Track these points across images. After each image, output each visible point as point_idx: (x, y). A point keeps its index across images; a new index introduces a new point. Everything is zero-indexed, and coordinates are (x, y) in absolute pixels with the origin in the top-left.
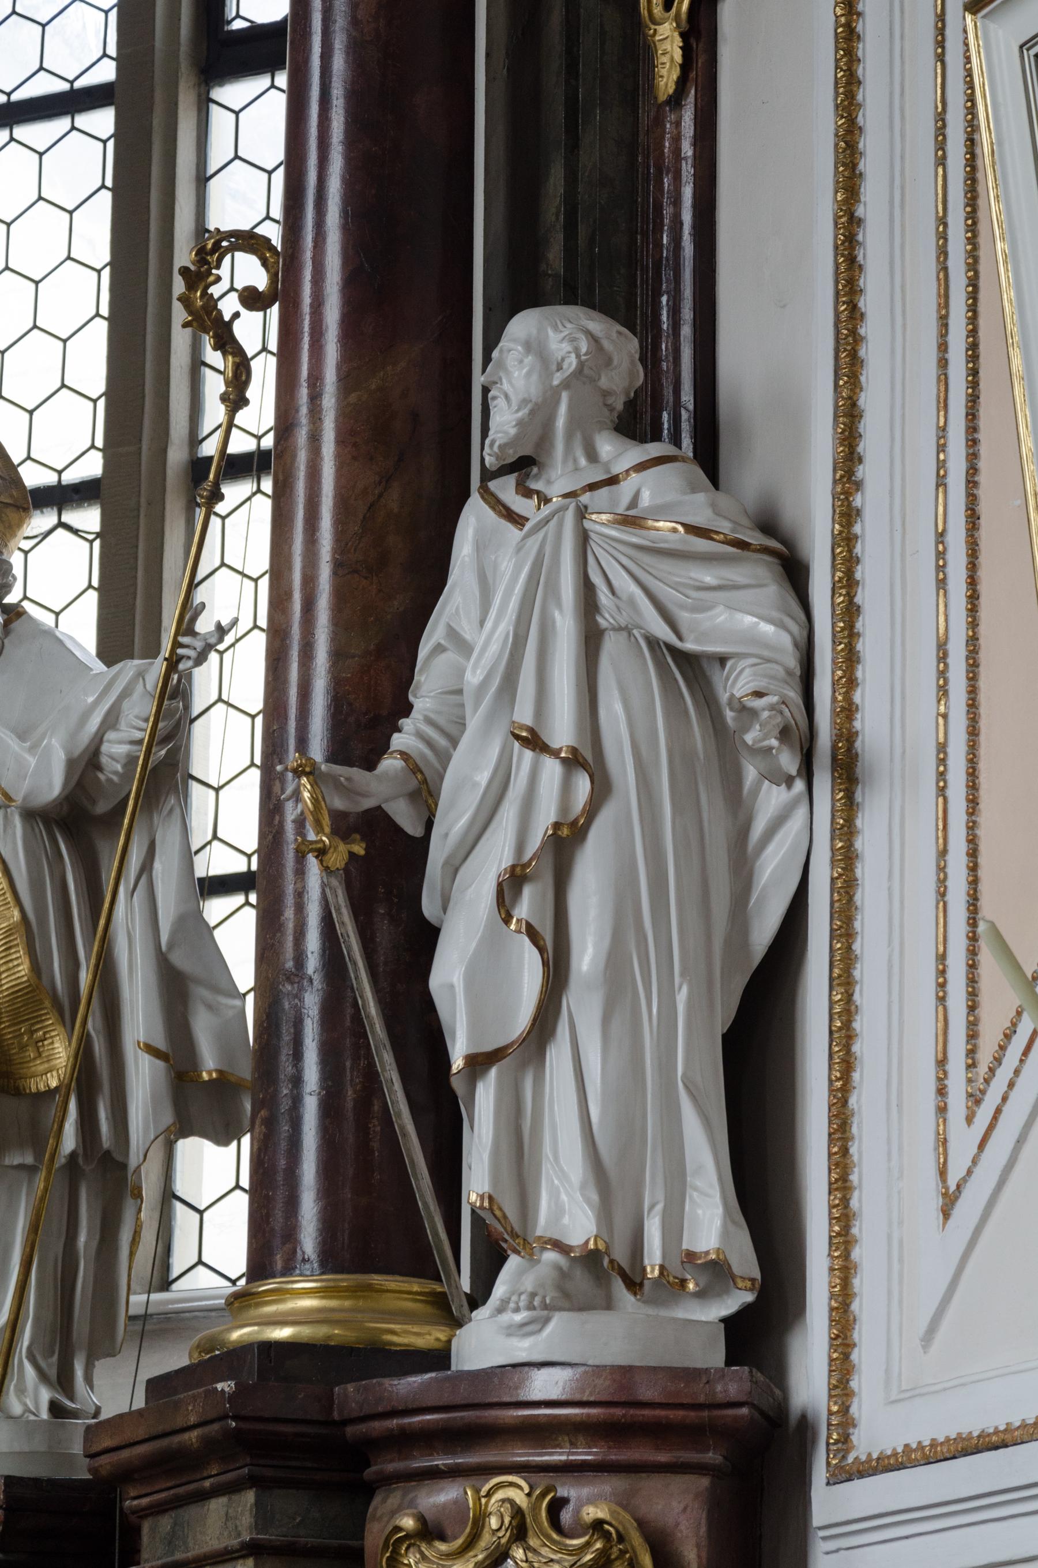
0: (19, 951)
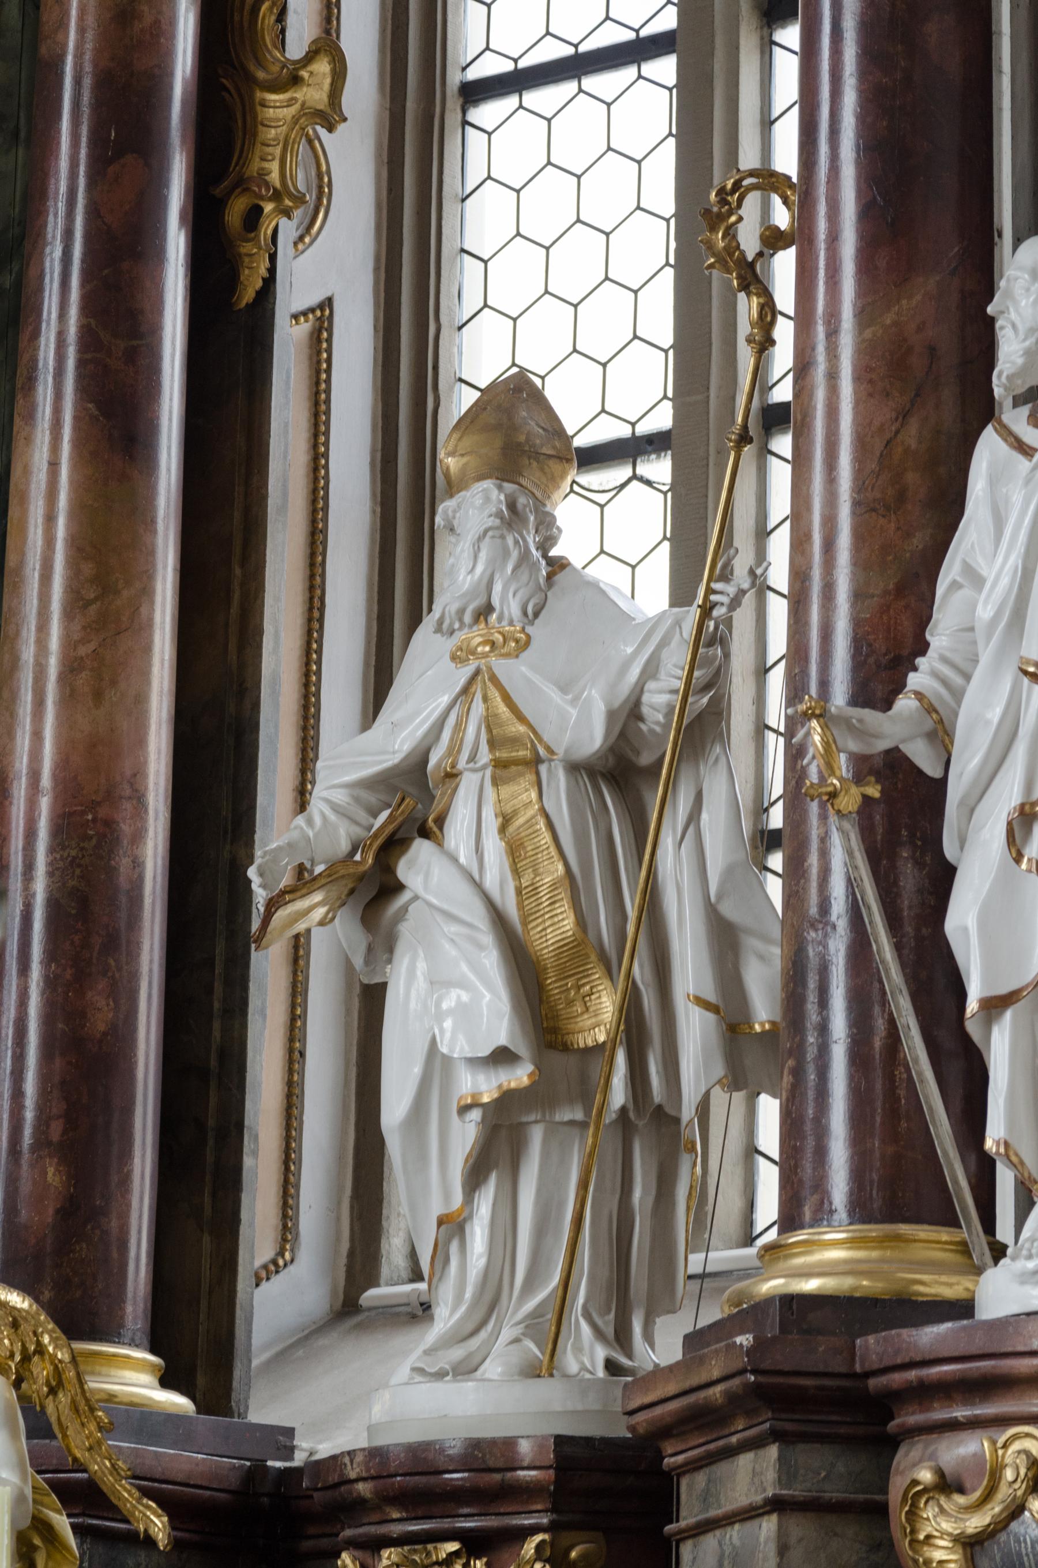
0: (564, 906)
